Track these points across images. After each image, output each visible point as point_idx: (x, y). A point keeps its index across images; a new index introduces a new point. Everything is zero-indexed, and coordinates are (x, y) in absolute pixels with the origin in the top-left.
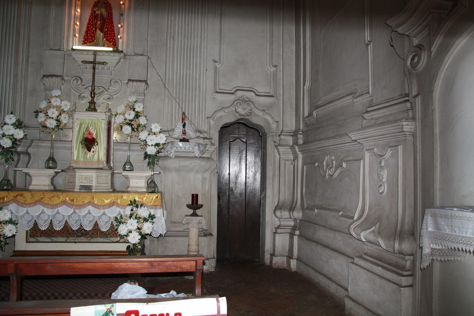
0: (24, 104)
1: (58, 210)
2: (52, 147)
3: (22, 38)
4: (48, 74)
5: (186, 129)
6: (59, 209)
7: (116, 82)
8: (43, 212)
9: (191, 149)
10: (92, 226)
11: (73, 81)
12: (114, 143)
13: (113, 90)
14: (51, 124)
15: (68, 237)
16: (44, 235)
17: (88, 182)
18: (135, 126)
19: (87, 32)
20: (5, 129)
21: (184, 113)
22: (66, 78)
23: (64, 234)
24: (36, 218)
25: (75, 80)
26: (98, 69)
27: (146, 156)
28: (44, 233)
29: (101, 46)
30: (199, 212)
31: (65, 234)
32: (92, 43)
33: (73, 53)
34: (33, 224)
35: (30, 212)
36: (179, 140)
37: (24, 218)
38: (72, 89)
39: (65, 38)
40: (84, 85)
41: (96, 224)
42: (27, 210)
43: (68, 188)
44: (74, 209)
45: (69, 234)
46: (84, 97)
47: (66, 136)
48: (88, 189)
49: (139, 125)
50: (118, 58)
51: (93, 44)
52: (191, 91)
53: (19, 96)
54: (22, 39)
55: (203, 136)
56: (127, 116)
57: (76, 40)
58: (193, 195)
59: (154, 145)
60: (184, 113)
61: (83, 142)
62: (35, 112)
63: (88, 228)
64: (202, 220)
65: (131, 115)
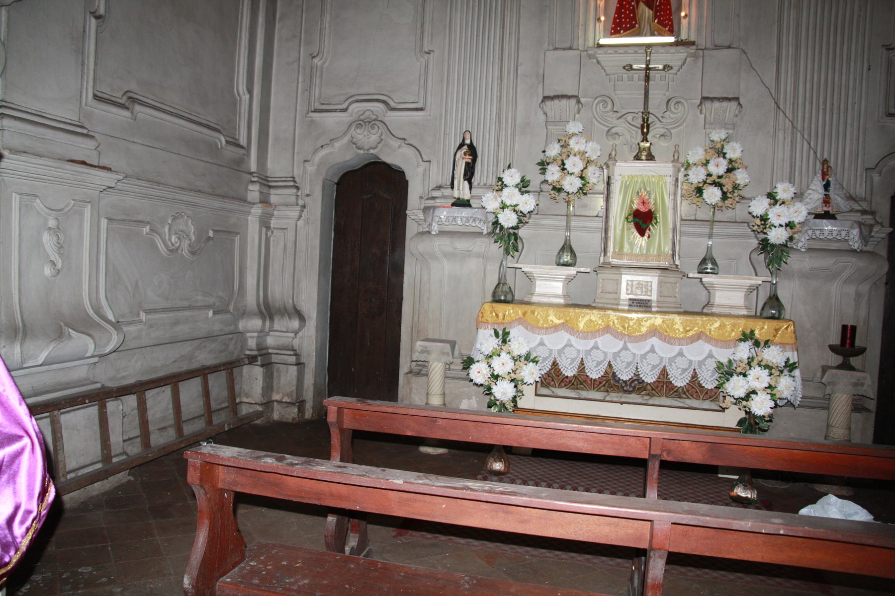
0: (513, 150)
1: (596, 342)
2: (568, 228)
3: (508, 32)
4: (552, 94)
5: (831, 193)
6: (598, 340)
7: (678, 103)
8: (569, 345)
9: (844, 233)
10: (547, 367)
11: (598, 103)
12: (682, 220)
13: (672, 118)
14: (571, 184)
15: (607, 391)
16: (565, 385)
17: (644, 293)
18: (728, 187)
19: (618, 11)
20: (507, 194)
21: (825, 162)
22: (582, 100)
23: (600, 386)
24: (696, 365)
25: (602, 102)
26: (622, 81)
27: (765, 245)
28: (566, 381)
29: (645, 35)
30: (854, 361)
31: (604, 385)
32: (631, 31)
33: (599, 52)
34: (690, 376)
35: (546, 342)
36: (813, 216)
37: (620, 357)
38: (594, 119)
39: (580, 26)
40: (617, 112)
41: (664, 373)
42: (542, 339)
43: (605, 303)
44: (625, 342)
45: (611, 386)
46: (616, 133)
47: (585, 206)
48: (645, 306)
49: (736, 187)
50: (683, 56)
51: (633, 32)
52: (835, 116)
53: (504, 135)
54: (508, 35)
55: (860, 208)
56: (712, 168)
57: (600, 27)
58: (844, 327)
59: (784, 225)
60: (825, 162)
61: (629, 217)
62: (539, 164)
63: (650, 378)
64: (865, 378)
65: (718, 167)
